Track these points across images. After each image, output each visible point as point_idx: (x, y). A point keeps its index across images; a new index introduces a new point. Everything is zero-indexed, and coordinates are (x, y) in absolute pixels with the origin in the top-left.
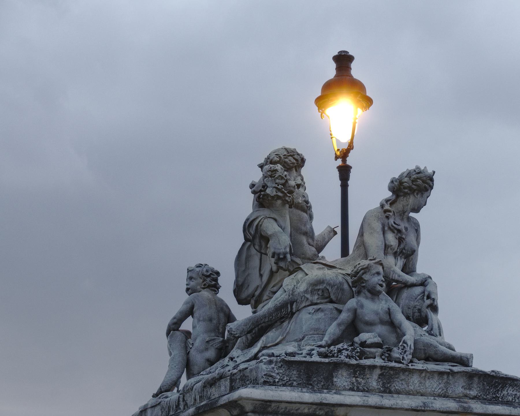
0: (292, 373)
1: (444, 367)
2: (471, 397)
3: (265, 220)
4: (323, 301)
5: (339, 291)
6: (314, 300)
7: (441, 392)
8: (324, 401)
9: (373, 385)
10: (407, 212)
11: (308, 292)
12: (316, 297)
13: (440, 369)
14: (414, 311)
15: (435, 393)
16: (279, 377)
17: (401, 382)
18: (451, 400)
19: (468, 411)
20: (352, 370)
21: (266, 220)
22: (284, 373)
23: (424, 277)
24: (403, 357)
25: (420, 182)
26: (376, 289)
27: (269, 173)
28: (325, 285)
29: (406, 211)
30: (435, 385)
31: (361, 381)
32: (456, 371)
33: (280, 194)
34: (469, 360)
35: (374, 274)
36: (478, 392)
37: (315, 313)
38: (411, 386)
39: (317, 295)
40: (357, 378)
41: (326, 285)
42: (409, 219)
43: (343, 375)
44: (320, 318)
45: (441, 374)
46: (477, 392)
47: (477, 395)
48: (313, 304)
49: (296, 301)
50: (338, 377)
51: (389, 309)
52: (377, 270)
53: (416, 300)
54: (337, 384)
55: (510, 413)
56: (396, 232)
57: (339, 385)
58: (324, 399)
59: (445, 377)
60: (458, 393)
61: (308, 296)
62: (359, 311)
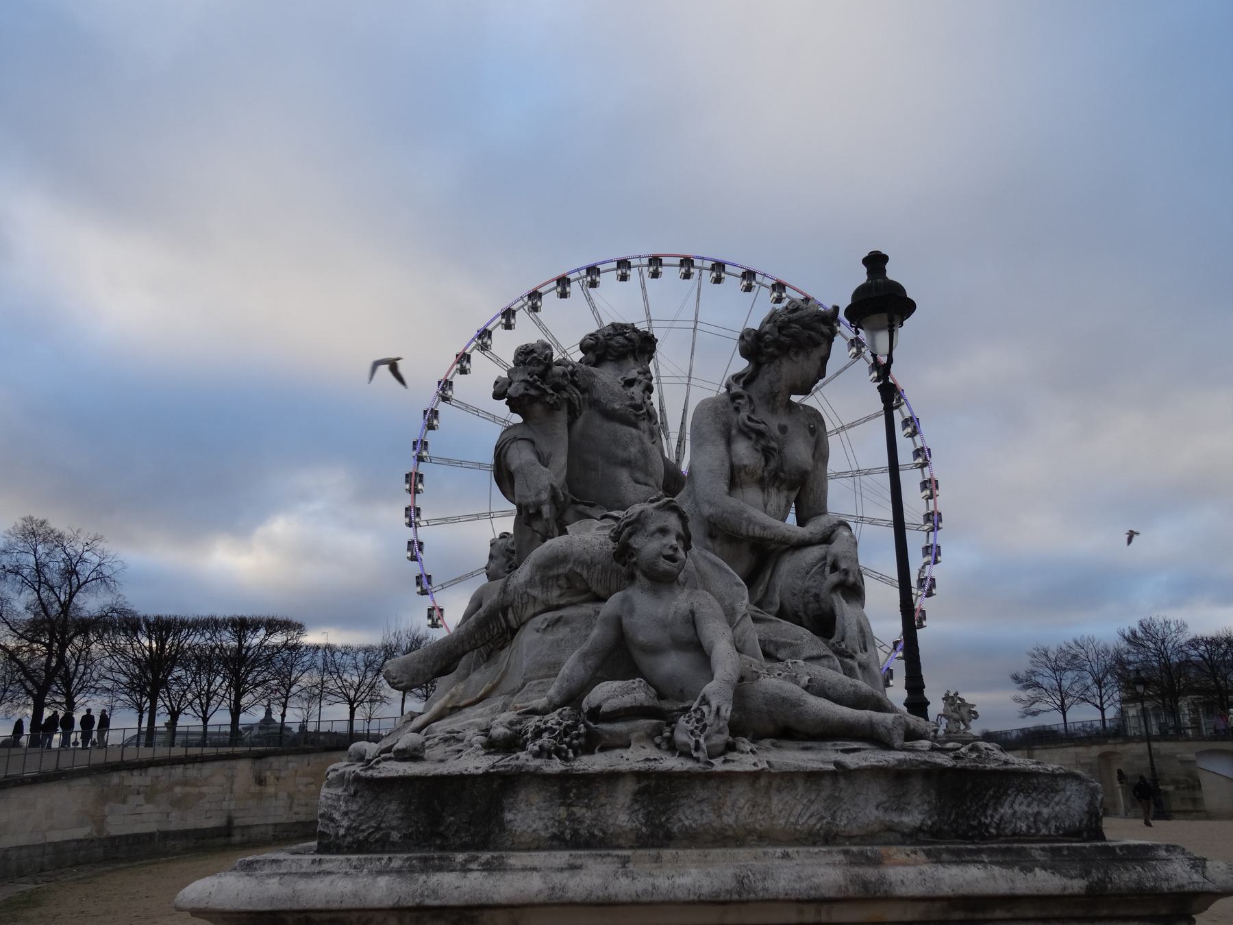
0: (385, 808)
1: (821, 756)
2: (906, 830)
3: (512, 445)
4: (575, 599)
5: (609, 574)
6: (552, 600)
7: (815, 825)
8: (429, 902)
9: (618, 822)
10: (780, 394)
11: (534, 583)
12: (556, 593)
13: (805, 765)
14: (806, 600)
15: (798, 827)
16: (345, 823)
17: (700, 806)
18: (835, 855)
19: (878, 894)
20: (556, 788)
21: (514, 445)
22: (362, 811)
23: (827, 525)
24: (697, 742)
25: (797, 328)
26: (656, 568)
27: (520, 358)
28: (570, 566)
29: (778, 392)
30: (800, 807)
31: (584, 814)
32: (853, 766)
33: (533, 392)
34: (891, 731)
35: (652, 534)
36: (923, 816)
37: (550, 629)
38: (728, 815)
39: (557, 588)
40: (574, 806)
41: (573, 565)
42: (791, 406)
43: (530, 803)
44: (562, 640)
45: (813, 777)
46: (920, 817)
47: (922, 824)
48: (549, 608)
49: (511, 605)
50: (516, 810)
51: (692, 612)
52: (660, 524)
53: (809, 576)
54: (515, 828)
55: (1010, 889)
56: (754, 436)
57: (519, 830)
58: (428, 896)
59: (827, 782)
60: (867, 822)
61: (536, 592)
62: (625, 621)
